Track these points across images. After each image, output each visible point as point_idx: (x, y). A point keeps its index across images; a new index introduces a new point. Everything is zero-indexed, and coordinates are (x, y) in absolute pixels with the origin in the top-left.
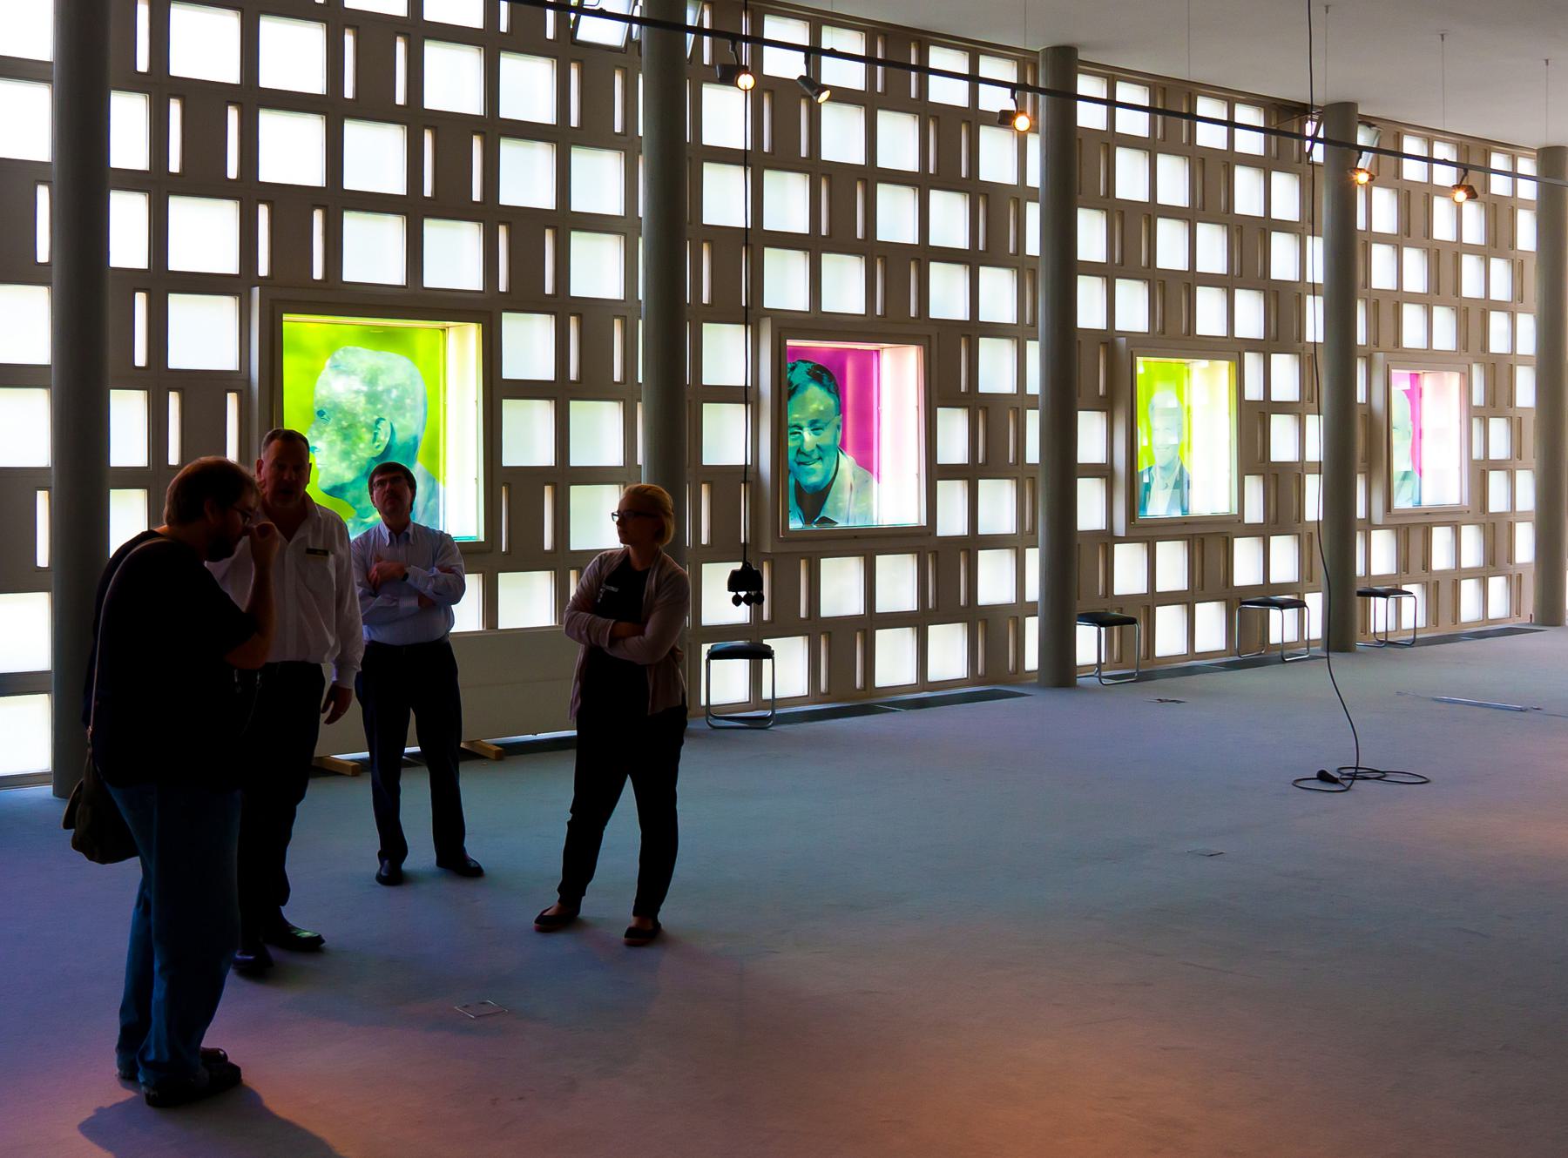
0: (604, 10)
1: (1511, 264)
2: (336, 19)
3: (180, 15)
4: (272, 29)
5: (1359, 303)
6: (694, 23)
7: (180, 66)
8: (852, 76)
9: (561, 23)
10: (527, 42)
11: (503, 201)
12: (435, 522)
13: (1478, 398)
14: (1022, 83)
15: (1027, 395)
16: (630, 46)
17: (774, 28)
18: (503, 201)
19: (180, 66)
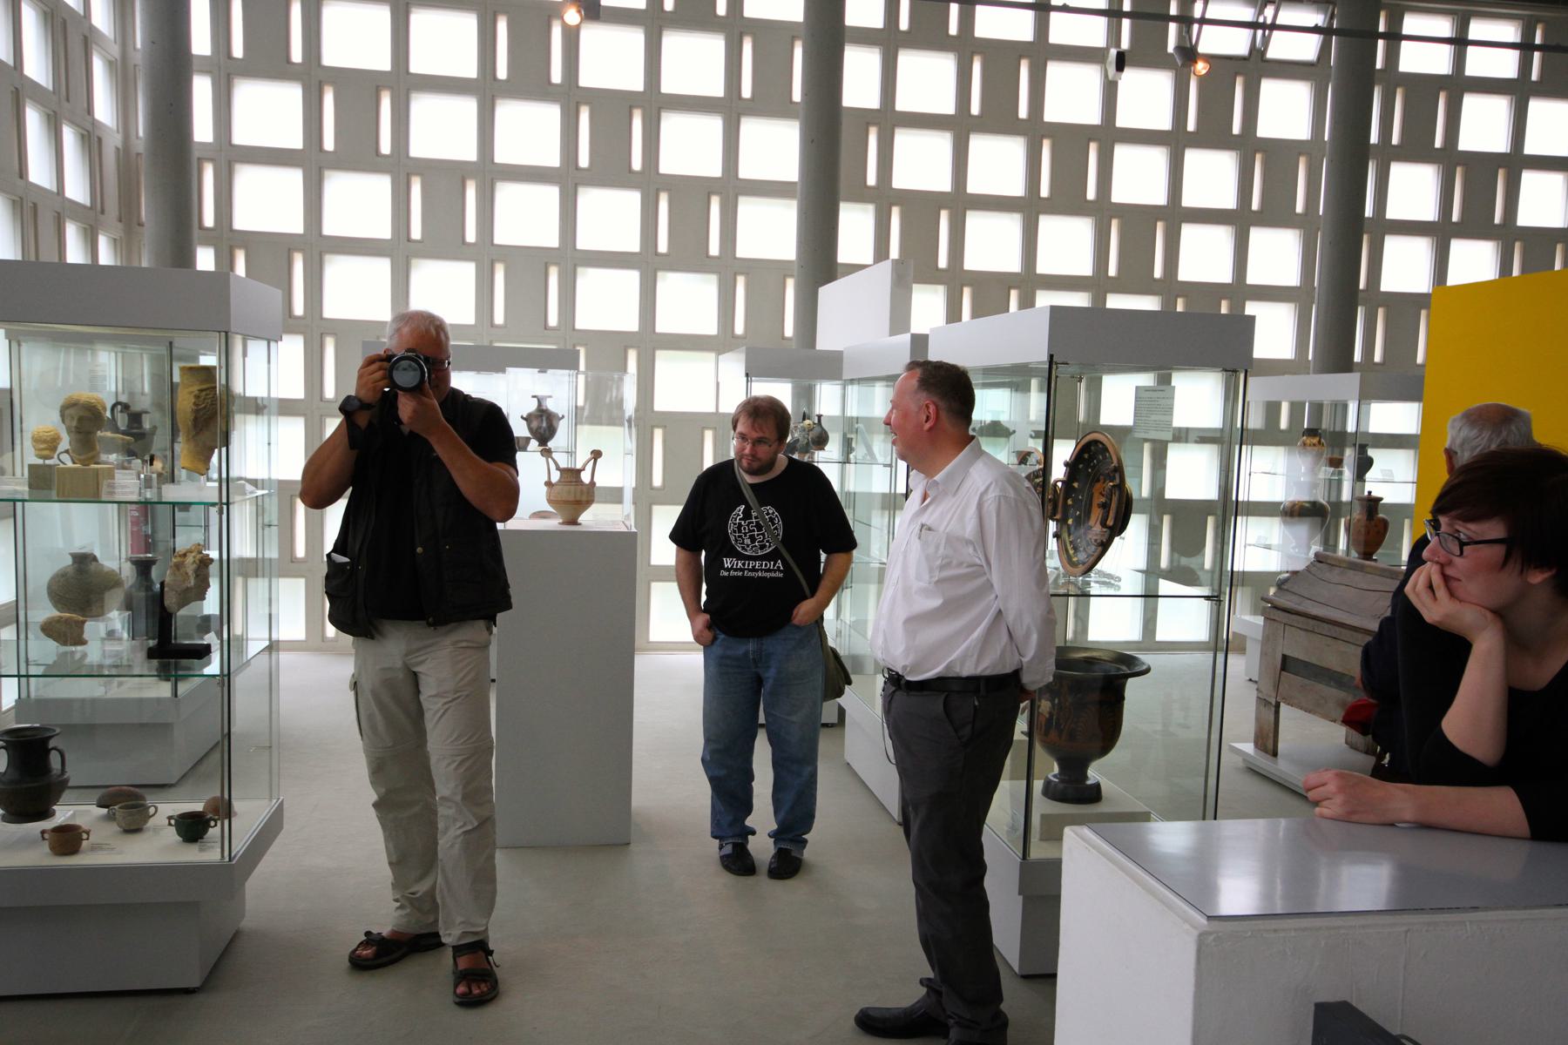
0: (1068, 6)
1: (53, 134)
2: (736, 27)
3: (331, 16)
4: (422, 21)
5: (1359, 309)
6: (1324, 23)
7: (333, 56)
8: (1505, 65)
9: (1184, 34)
10: (928, 35)
11: (1114, 199)
12: (1397, 545)
13: (1110, 522)
14: (1116, 8)
15: (304, 415)
16: (1254, 52)
17: (1412, 24)
18: (1114, 199)
19: (333, 56)
